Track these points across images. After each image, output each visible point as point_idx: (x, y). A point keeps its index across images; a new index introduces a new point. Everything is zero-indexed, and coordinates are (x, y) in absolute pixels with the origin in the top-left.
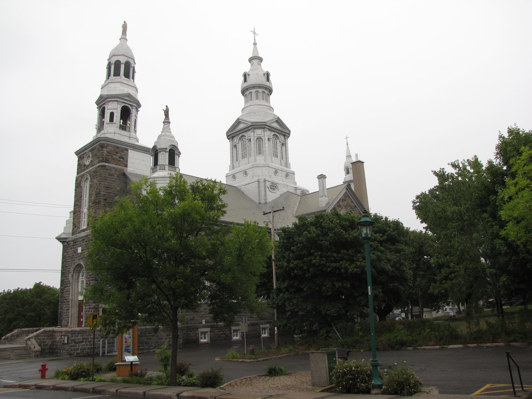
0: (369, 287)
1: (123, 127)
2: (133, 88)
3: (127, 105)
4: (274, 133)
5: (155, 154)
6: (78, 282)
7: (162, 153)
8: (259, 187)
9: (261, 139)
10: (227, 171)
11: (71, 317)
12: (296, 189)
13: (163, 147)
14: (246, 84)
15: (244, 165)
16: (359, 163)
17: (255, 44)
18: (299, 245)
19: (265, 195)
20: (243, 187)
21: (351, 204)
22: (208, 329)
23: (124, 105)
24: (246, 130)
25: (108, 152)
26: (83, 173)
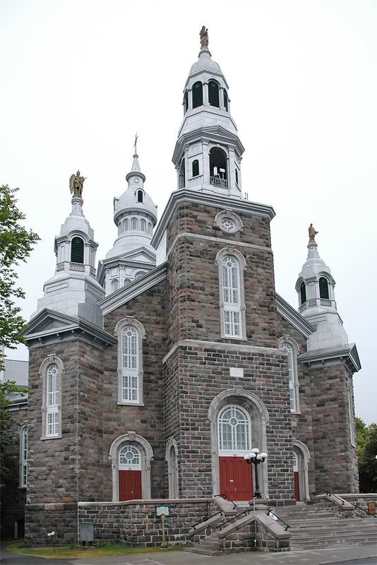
0: (52, 431)
1: (214, 180)
3: (218, 146)
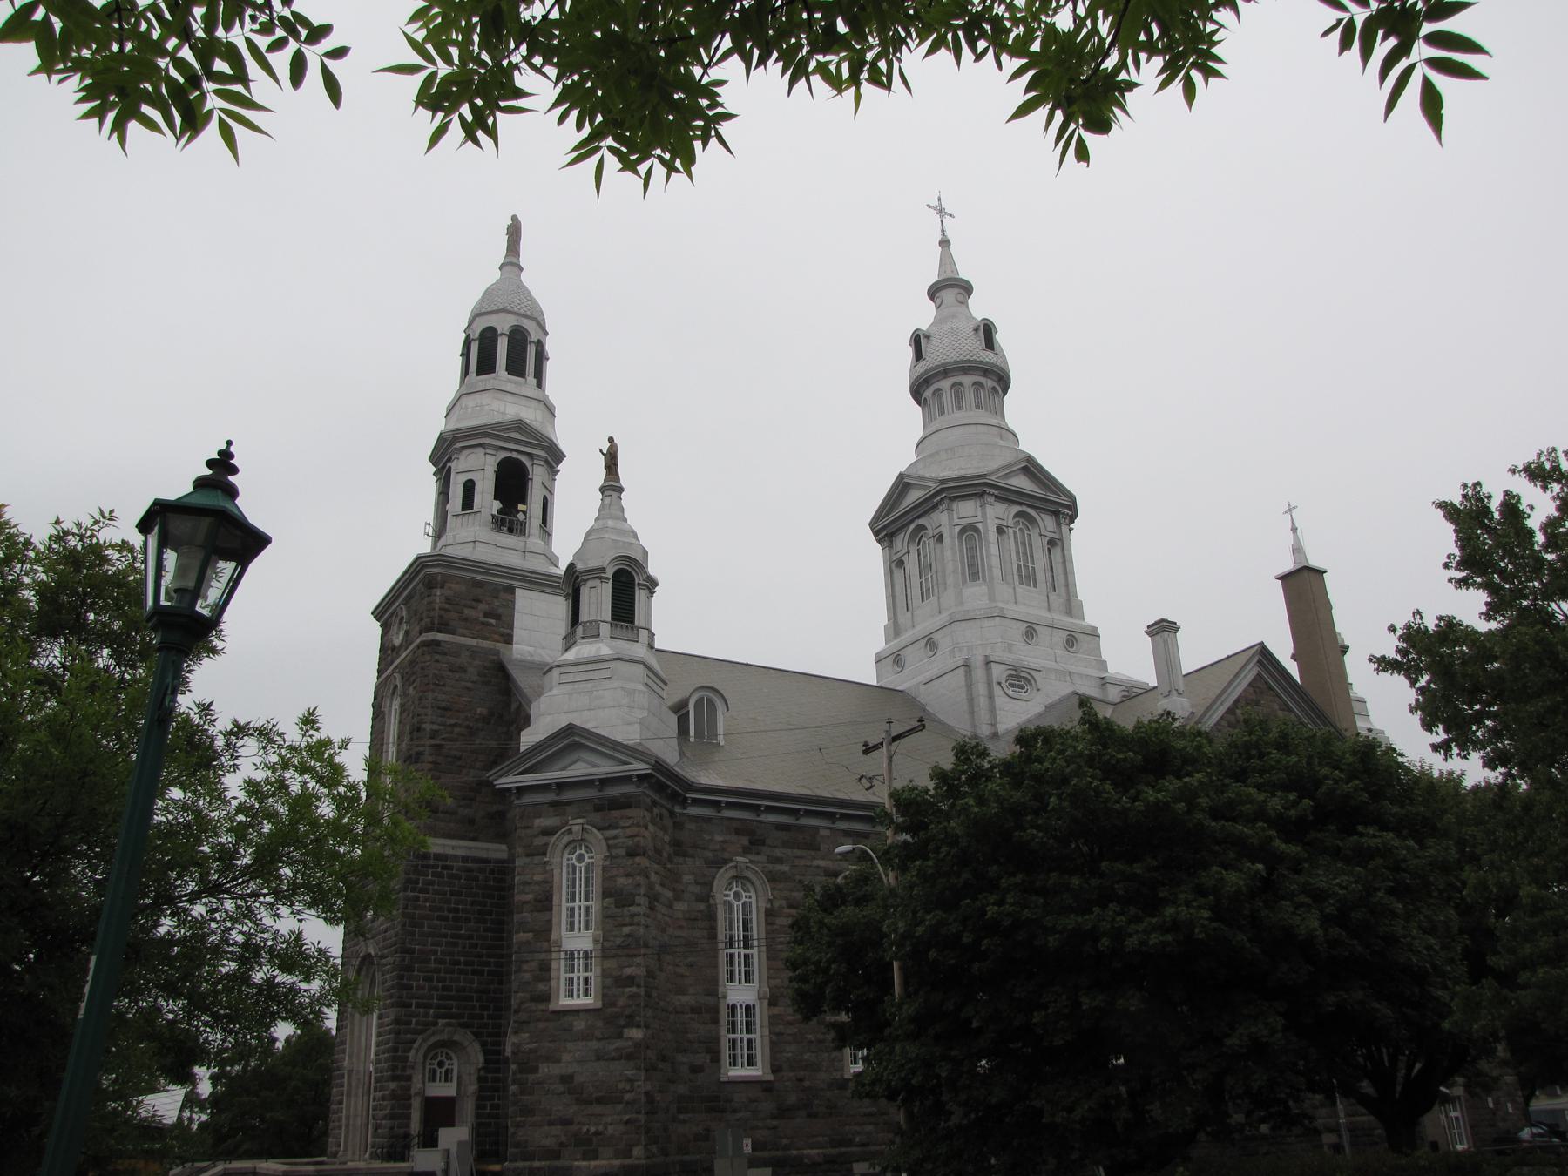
2: (534, 404)
3: (514, 455)
4: (1018, 508)
7: (590, 583)
8: (969, 685)
9: (976, 530)
10: (878, 643)
11: (347, 1126)
12: (1104, 682)
13: (593, 564)
14: (923, 366)
15: (926, 619)
16: (1305, 574)
17: (945, 243)
18: (945, 849)
19: (992, 709)
20: (922, 688)
21: (1280, 714)
24: (928, 505)
25: (448, 601)
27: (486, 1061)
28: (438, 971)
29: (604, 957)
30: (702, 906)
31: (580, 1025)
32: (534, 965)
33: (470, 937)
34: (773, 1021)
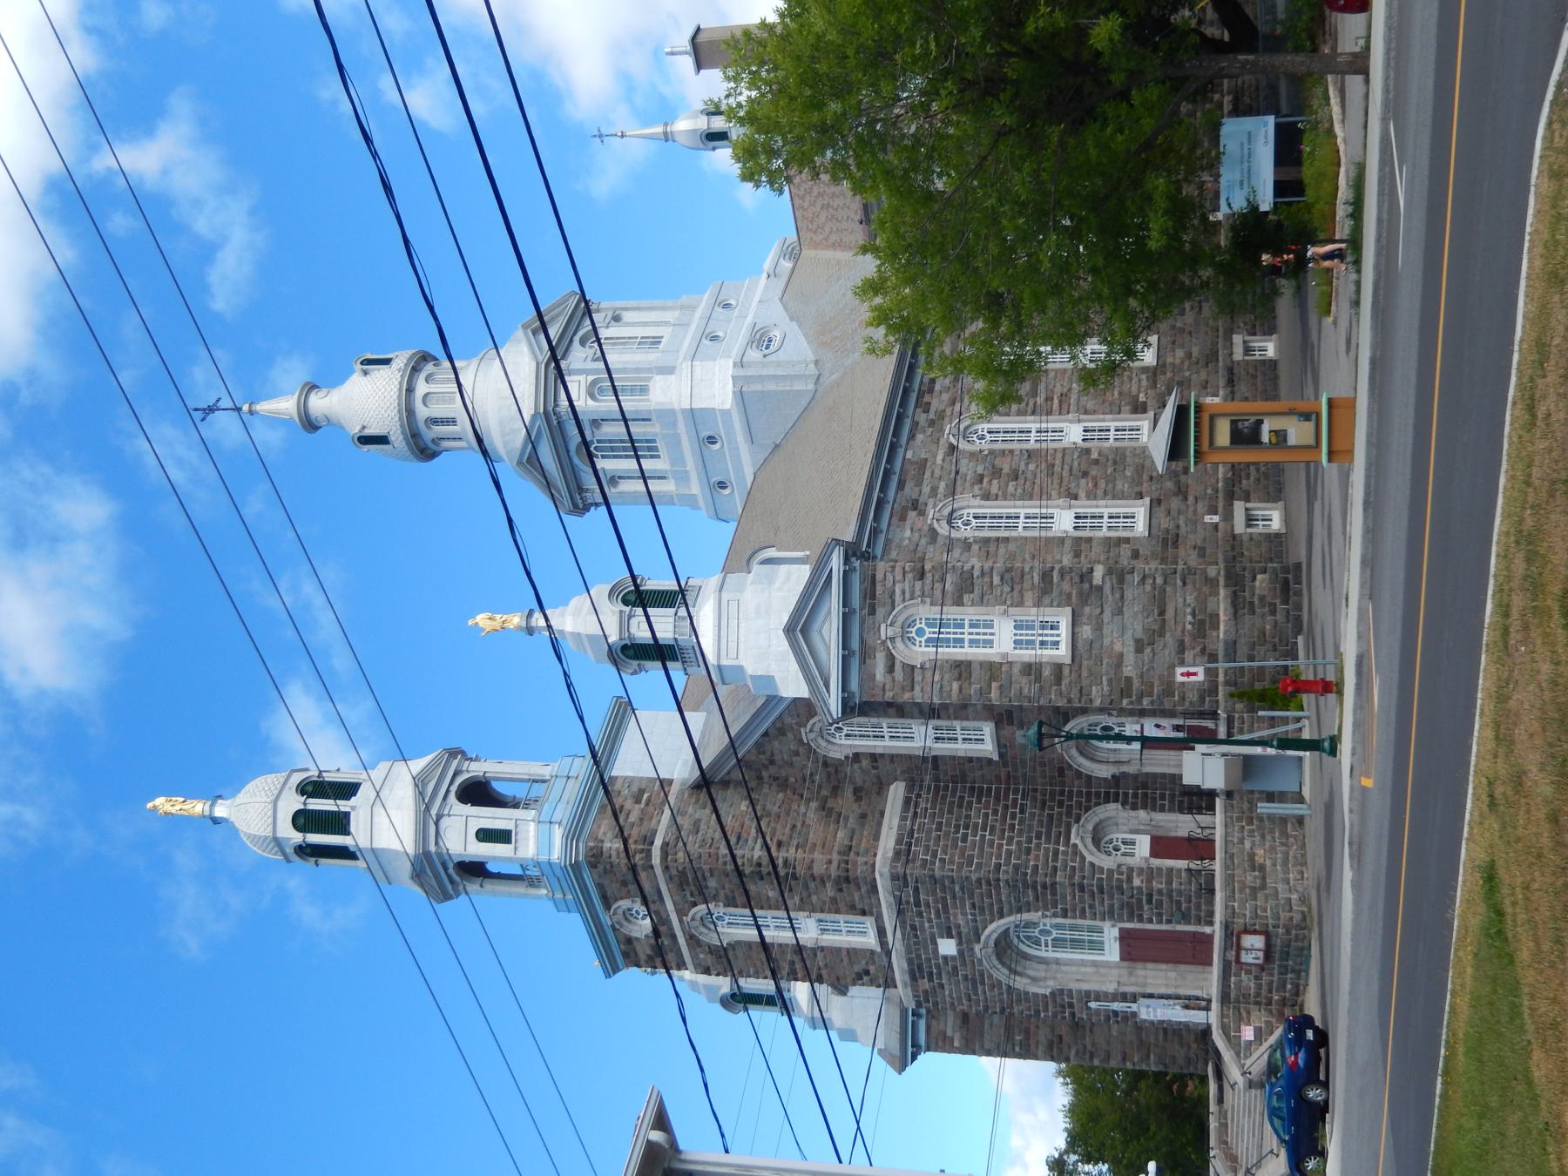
3: (454, 788)
5: (636, 657)
6: (1057, 962)
22: (1239, 507)
23: (452, 797)
26: (682, 941)
27: (1116, 801)
28: (1019, 843)
29: (1021, 604)
30: (975, 547)
31: (1086, 631)
32: (1024, 680)
33: (986, 815)
34: (1091, 496)
